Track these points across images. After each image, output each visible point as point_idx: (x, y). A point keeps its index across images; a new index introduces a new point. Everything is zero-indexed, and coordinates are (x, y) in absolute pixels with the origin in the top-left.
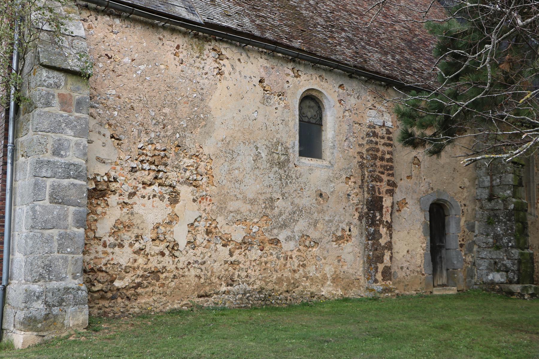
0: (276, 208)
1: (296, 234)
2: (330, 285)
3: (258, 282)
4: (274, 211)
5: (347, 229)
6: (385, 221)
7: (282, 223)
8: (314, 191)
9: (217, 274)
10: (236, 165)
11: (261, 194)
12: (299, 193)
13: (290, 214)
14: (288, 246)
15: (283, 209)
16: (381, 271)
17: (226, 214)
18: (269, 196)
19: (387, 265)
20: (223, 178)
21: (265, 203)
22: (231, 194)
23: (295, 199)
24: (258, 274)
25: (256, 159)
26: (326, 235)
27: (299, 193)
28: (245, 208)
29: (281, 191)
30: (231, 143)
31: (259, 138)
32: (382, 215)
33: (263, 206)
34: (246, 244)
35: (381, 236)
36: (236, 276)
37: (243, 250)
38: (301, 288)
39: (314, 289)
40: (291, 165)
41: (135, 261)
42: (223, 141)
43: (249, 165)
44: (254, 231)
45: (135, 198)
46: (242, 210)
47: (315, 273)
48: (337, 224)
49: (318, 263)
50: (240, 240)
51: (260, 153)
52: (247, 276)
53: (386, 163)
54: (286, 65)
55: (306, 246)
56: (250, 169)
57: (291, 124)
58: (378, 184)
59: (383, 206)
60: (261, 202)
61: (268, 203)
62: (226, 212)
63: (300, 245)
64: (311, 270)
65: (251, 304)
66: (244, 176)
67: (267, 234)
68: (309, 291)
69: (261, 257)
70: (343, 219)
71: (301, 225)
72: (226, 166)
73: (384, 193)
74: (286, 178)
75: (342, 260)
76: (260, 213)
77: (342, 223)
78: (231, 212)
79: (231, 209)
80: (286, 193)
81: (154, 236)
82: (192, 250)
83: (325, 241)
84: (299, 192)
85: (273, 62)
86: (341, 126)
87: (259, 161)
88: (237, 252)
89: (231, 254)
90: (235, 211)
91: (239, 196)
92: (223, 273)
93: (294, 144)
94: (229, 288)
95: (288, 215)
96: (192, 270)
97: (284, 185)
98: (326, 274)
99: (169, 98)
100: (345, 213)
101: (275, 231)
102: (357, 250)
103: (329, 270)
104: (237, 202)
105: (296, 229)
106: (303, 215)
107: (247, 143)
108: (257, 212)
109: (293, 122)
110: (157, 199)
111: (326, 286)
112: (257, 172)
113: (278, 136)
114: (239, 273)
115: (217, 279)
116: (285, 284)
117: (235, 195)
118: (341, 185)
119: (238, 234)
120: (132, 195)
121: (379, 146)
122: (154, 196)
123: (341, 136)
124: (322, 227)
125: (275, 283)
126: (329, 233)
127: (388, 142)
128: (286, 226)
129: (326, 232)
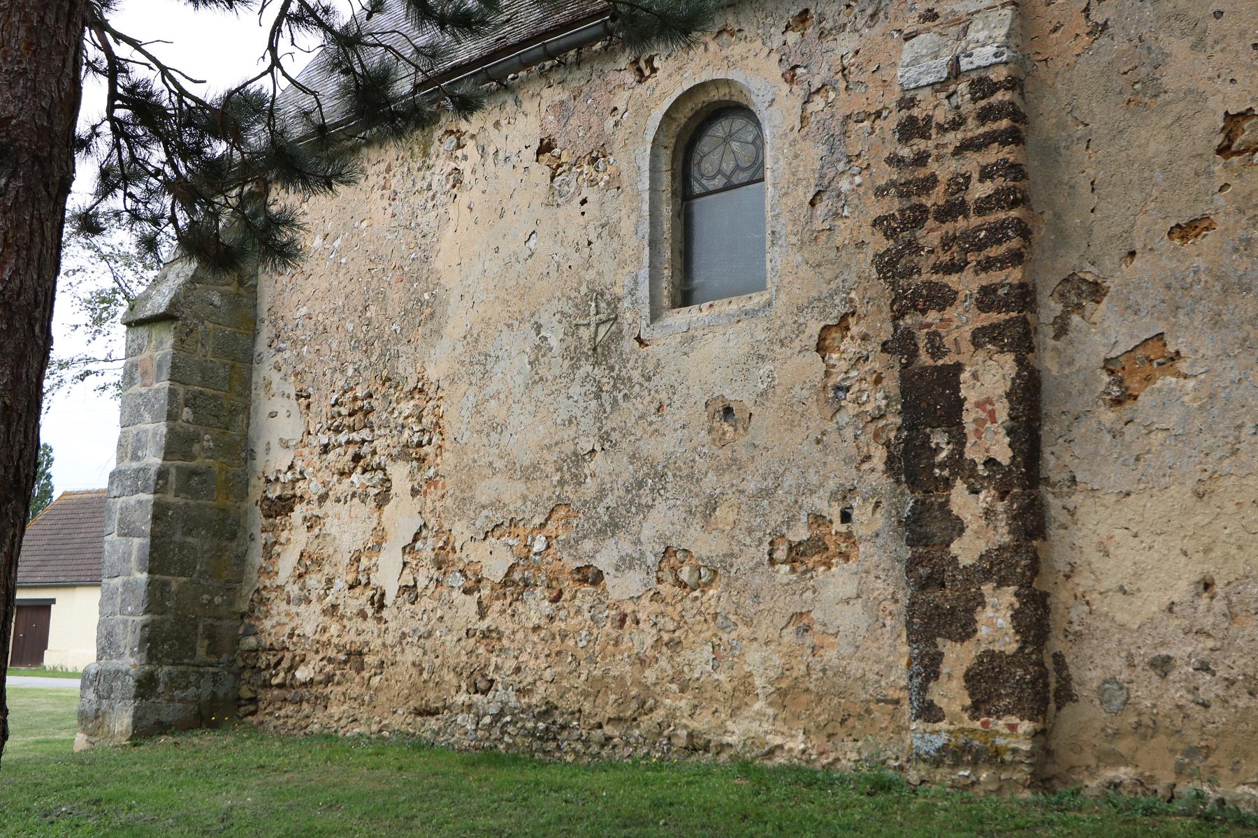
0: (588, 480)
1: (647, 548)
2: (760, 714)
3: (541, 687)
4: (582, 489)
5: (834, 512)
6: (979, 458)
7: (606, 518)
8: (702, 405)
9: (452, 662)
10: (492, 388)
11: (549, 447)
12: (651, 424)
13: (628, 491)
14: (624, 586)
15: (607, 479)
16: (960, 672)
17: (472, 515)
18: (568, 448)
19: (997, 648)
20: (463, 427)
21: (559, 469)
22: (482, 463)
23: (641, 443)
24: (543, 666)
25: (537, 359)
26: (748, 541)
27: (651, 424)
28: (511, 492)
29: (599, 429)
30: (482, 337)
31: (544, 300)
32: (959, 439)
33: (556, 478)
34: (514, 585)
35: (958, 527)
36: (492, 668)
37: (509, 600)
38: (659, 715)
39: (702, 723)
40: (629, 344)
41: (324, 630)
42: (465, 338)
43: (520, 380)
44: (535, 550)
45: (328, 503)
46: (506, 498)
47: (709, 668)
48: (791, 499)
49: (725, 637)
50: (499, 576)
51: (546, 339)
52: (518, 670)
53: (975, 221)
54: (610, 66)
55: (683, 585)
56: (522, 388)
57: (626, 226)
58: (933, 316)
59: (961, 402)
60: (550, 469)
61: (569, 468)
62: (473, 507)
63: (659, 581)
64: (698, 658)
65: (508, 744)
66: (509, 409)
67: (566, 558)
68: (686, 727)
69: (551, 619)
70: (814, 479)
71: (660, 522)
72: (471, 398)
73: (967, 346)
74: (614, 386)
75: (817, 627)
76: (550, 499)
77: (812, 492)
78: (484, 507)
79: (484, 499)
80: (614, 429)
81: (350, 578)
82: (408, 605)
83: (743, 562)
84: (653, 418)
85: (577, 78)
86: (796, 156)
87: (542, 360)
88: (497, 605)
89: (482, 615)
90: (492, 504)
91: (499, 464)
92: (464, 658)
93: (636, 282)
94: (477, 697)
95: (622, 493)
96: (408, 649)
97: (608, 410)
98: (751, 675)
99: (374, 283)
100: (834, 458)
101: (588, 545)
102: (880, 588)
103: (759, 663)
104: (495, 479)
105: (647, 533)
106: (669, 486)
107: (516, 323)
108: (540, 496)
109: (633, 217)
110: (356, 500)
111: (745, 713)
112: (538, 391)
113: (591, 275)
114: (499, 660)
115: (452, 674)
116: (613, 697)
117: (491, 463)
118: (798, 360)
119: (495, 561)
120: (323, 498)
121: (933, 166)
122: (354, 495)
123: (801, 191)
124: (732, 517)
125: (586, 695)
126: (759, 534)
127: (982, 130)
128: (616, 526)
129: (750, 531)
